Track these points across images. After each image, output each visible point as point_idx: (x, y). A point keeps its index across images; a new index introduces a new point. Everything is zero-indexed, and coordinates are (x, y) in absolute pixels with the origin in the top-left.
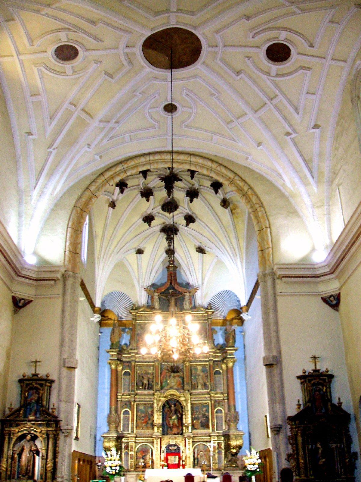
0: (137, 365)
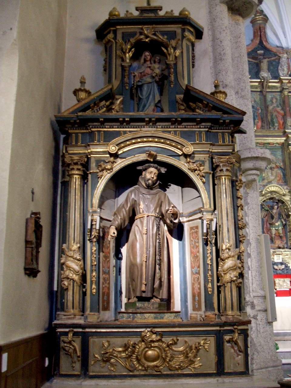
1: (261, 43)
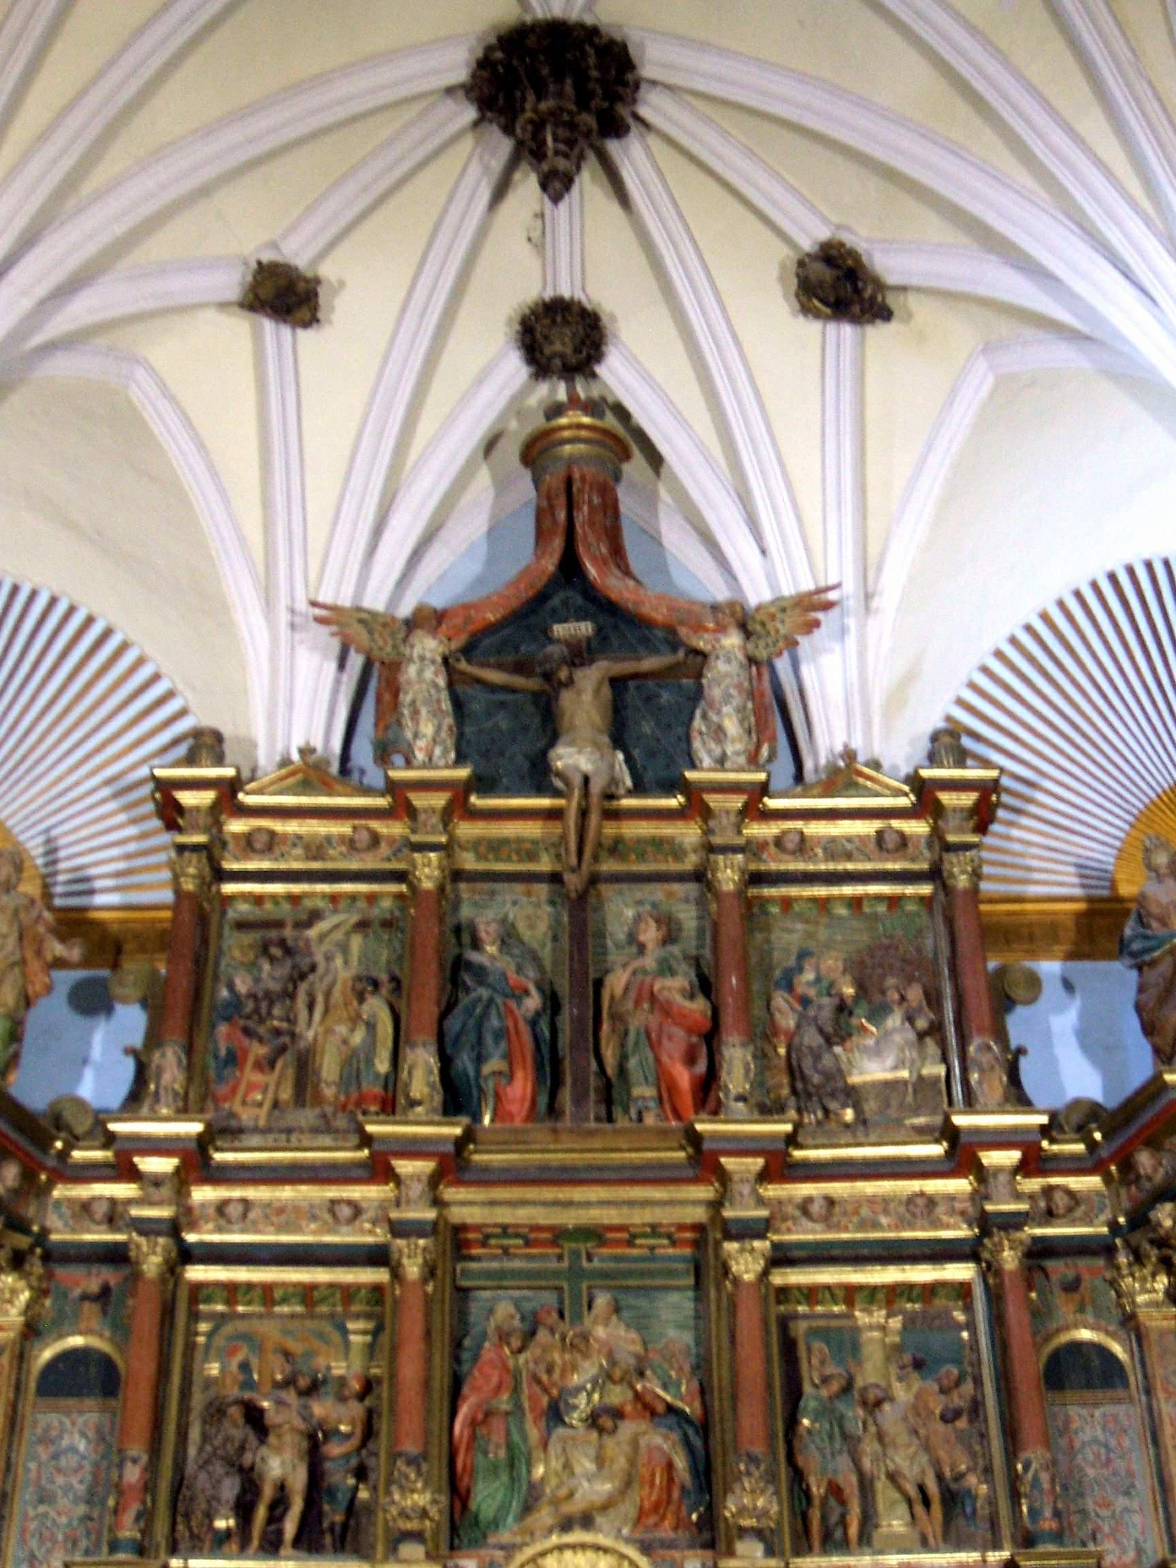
0: (199, 1291)
1: (570, 566)
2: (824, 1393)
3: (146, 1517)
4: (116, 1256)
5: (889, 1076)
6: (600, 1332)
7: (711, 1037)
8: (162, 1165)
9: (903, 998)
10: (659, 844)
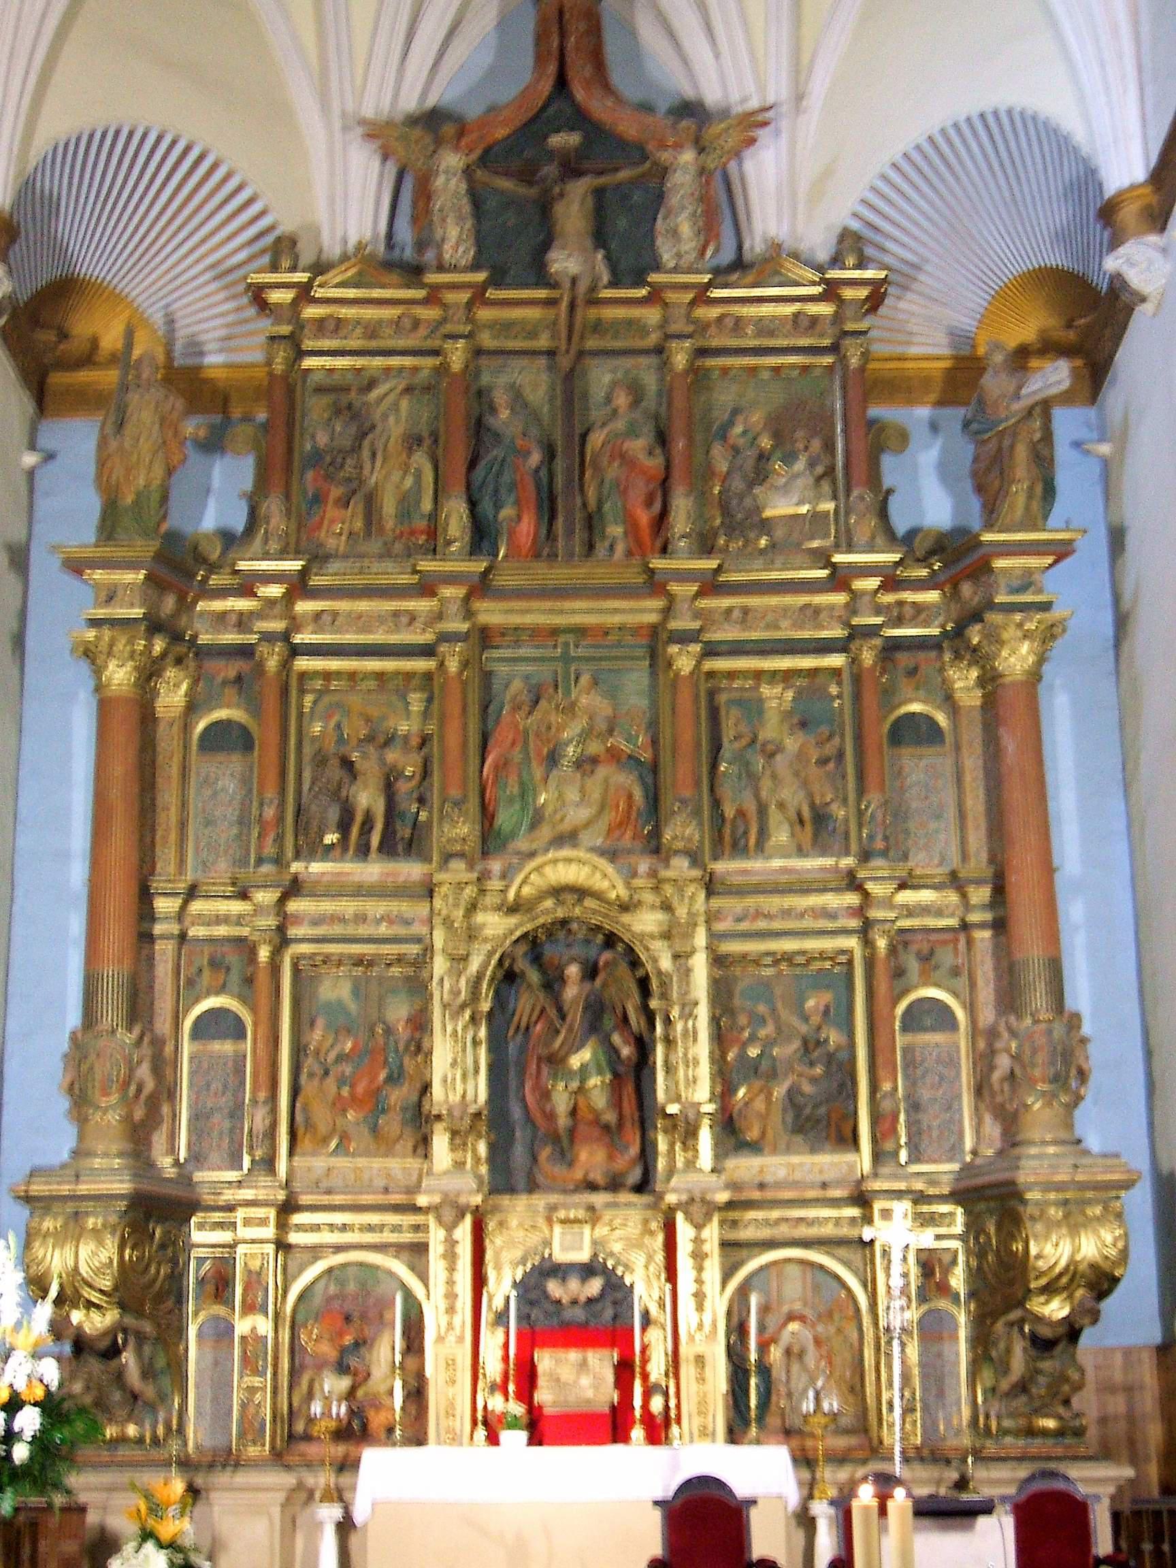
0: (303, 676)
2: (737, 745)
3: (280, 839)
4: (245, 651)
5: (791, 511)
6: (584, 701)
7: (665, 485)
8: (275, 591)
9: (806, 448)
10: (630, 323)
